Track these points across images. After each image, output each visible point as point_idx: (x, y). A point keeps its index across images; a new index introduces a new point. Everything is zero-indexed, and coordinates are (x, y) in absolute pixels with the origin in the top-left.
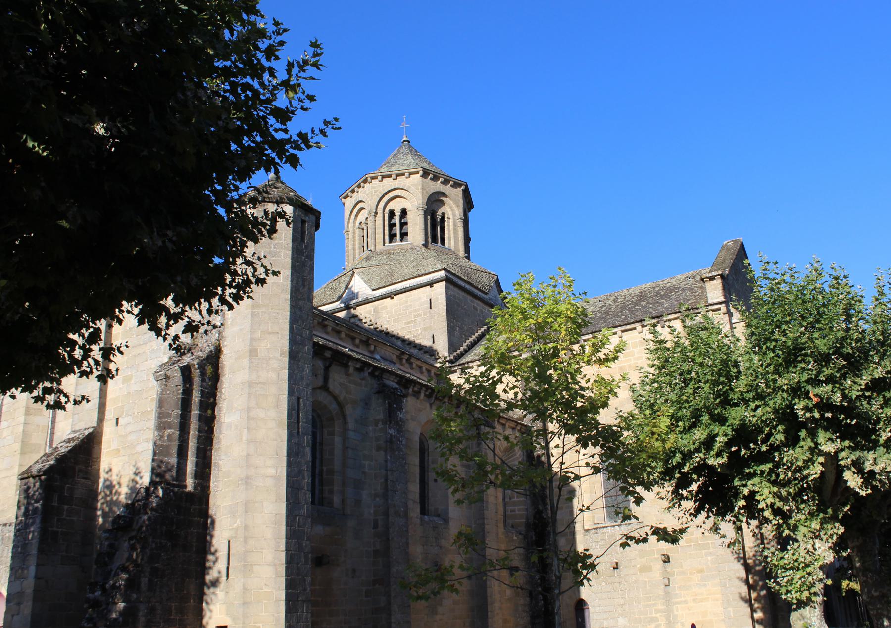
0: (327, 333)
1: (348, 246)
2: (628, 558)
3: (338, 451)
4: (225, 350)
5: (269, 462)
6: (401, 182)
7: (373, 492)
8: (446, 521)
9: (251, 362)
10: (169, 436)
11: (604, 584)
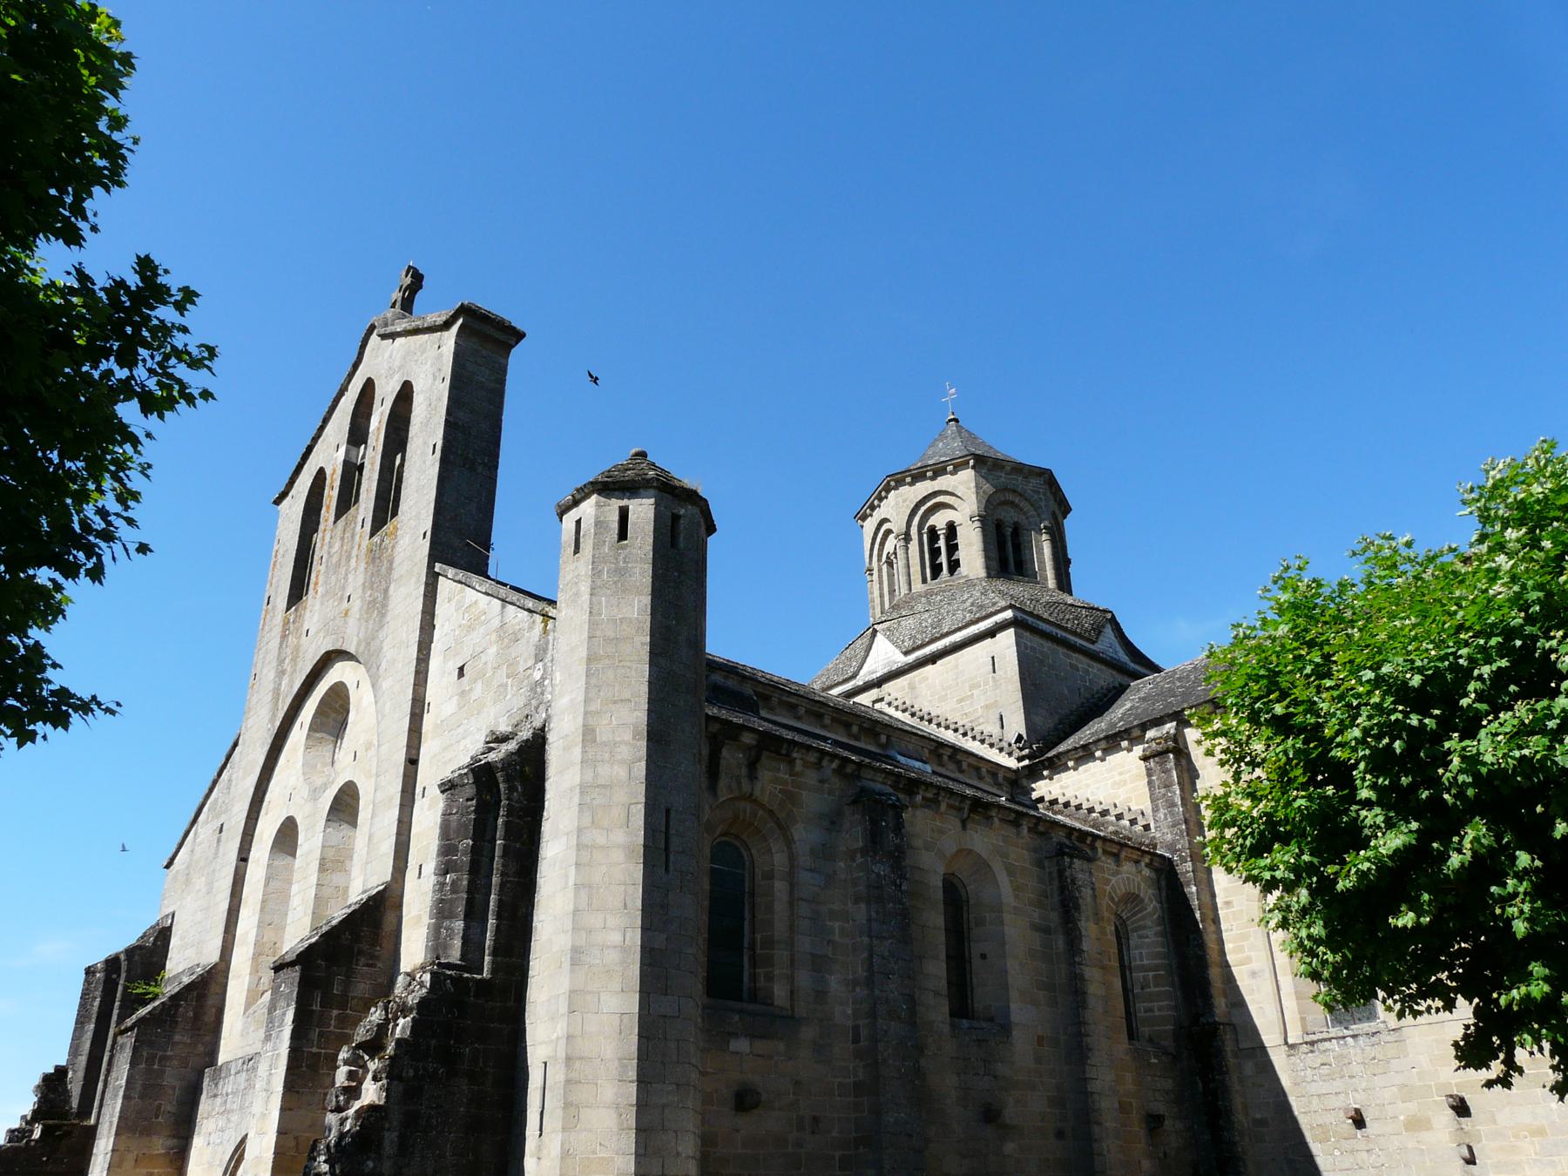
0: (799, 718)
1: (872, 593)
2: (1378, 1102)
3: (780, 907)
4: (551, 737)
5: (612, 921)
6: (943, 482)
7: (851, 977)
8: (1006, 1028)
9: (584, 752)
10: (453, 882)
11: (1337, 1153)
